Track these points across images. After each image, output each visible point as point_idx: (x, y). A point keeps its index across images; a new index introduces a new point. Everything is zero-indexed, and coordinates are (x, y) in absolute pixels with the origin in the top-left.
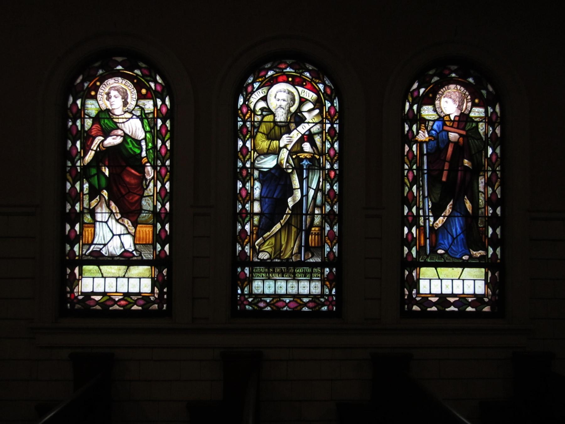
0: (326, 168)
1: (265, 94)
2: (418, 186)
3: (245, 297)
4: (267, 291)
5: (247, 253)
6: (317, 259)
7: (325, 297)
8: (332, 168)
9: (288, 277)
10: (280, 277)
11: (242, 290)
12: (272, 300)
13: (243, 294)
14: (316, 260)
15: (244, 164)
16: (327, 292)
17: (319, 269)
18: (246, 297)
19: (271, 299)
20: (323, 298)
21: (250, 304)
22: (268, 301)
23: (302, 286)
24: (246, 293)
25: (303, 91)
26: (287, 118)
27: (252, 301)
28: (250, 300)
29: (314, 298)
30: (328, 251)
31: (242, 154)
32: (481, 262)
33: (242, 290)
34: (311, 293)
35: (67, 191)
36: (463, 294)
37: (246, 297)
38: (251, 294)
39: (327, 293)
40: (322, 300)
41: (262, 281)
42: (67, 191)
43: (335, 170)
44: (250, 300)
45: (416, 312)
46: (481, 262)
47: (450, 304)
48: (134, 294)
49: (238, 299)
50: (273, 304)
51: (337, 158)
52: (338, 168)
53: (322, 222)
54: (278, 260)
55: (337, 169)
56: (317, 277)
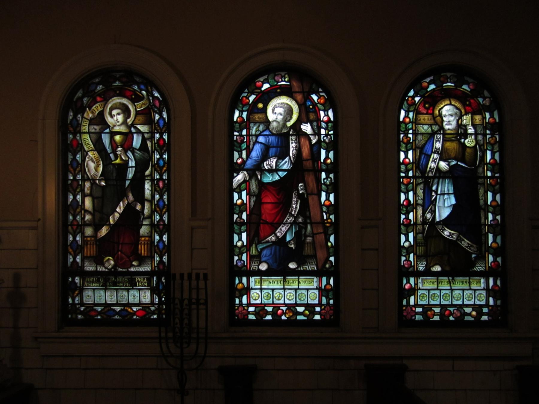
0: (156, 178)
1: (102, 109)
2: (248, 192)
3: (76, 307)
4: (98, 301)
5: (78, 262)
6: (138, 268)
7: (155, 306)
8: (161, 178)
9: (99, 287)
10: (93, 286)
11: (73, 300)
12: (103, 309)
13: (74, 304)
14: (145, 269)
15: (75, 177)
16: (157, 302)
17: (126, 278)
18: (77, 306)
19: (103, 307)
20: (153, 306)
21: (81, 313)
22: (100, 310)
23: (113, 297)
24: (77, 302)
25: (96, 107)
26: (278, 125)
27: (84, 309)
28: (82, 309)
29: (145, 307)
30: (158, 261)
31: (72, 167)
32: (130, 277)
33: (73, 300)
34: (141, 302)
35: (69, 203)
36: (261, 303)
37: (77, 306)
38: (82, 304)
39: (157, 303)
40: (153, 308)
41: (93, 291)
42: (69, 203)
43: (164, 180)
44: (82, 309)
45: (252, 320)
46: (130, 277)
47: (267, 313)
48: (487, 281)
49: (70, 308)
50: (104, 313)
51: (166, 168)
52: (166, 178)
53: (151, 232)
54: (157, 269)
55: (165, 179)
56: (142, 286)
